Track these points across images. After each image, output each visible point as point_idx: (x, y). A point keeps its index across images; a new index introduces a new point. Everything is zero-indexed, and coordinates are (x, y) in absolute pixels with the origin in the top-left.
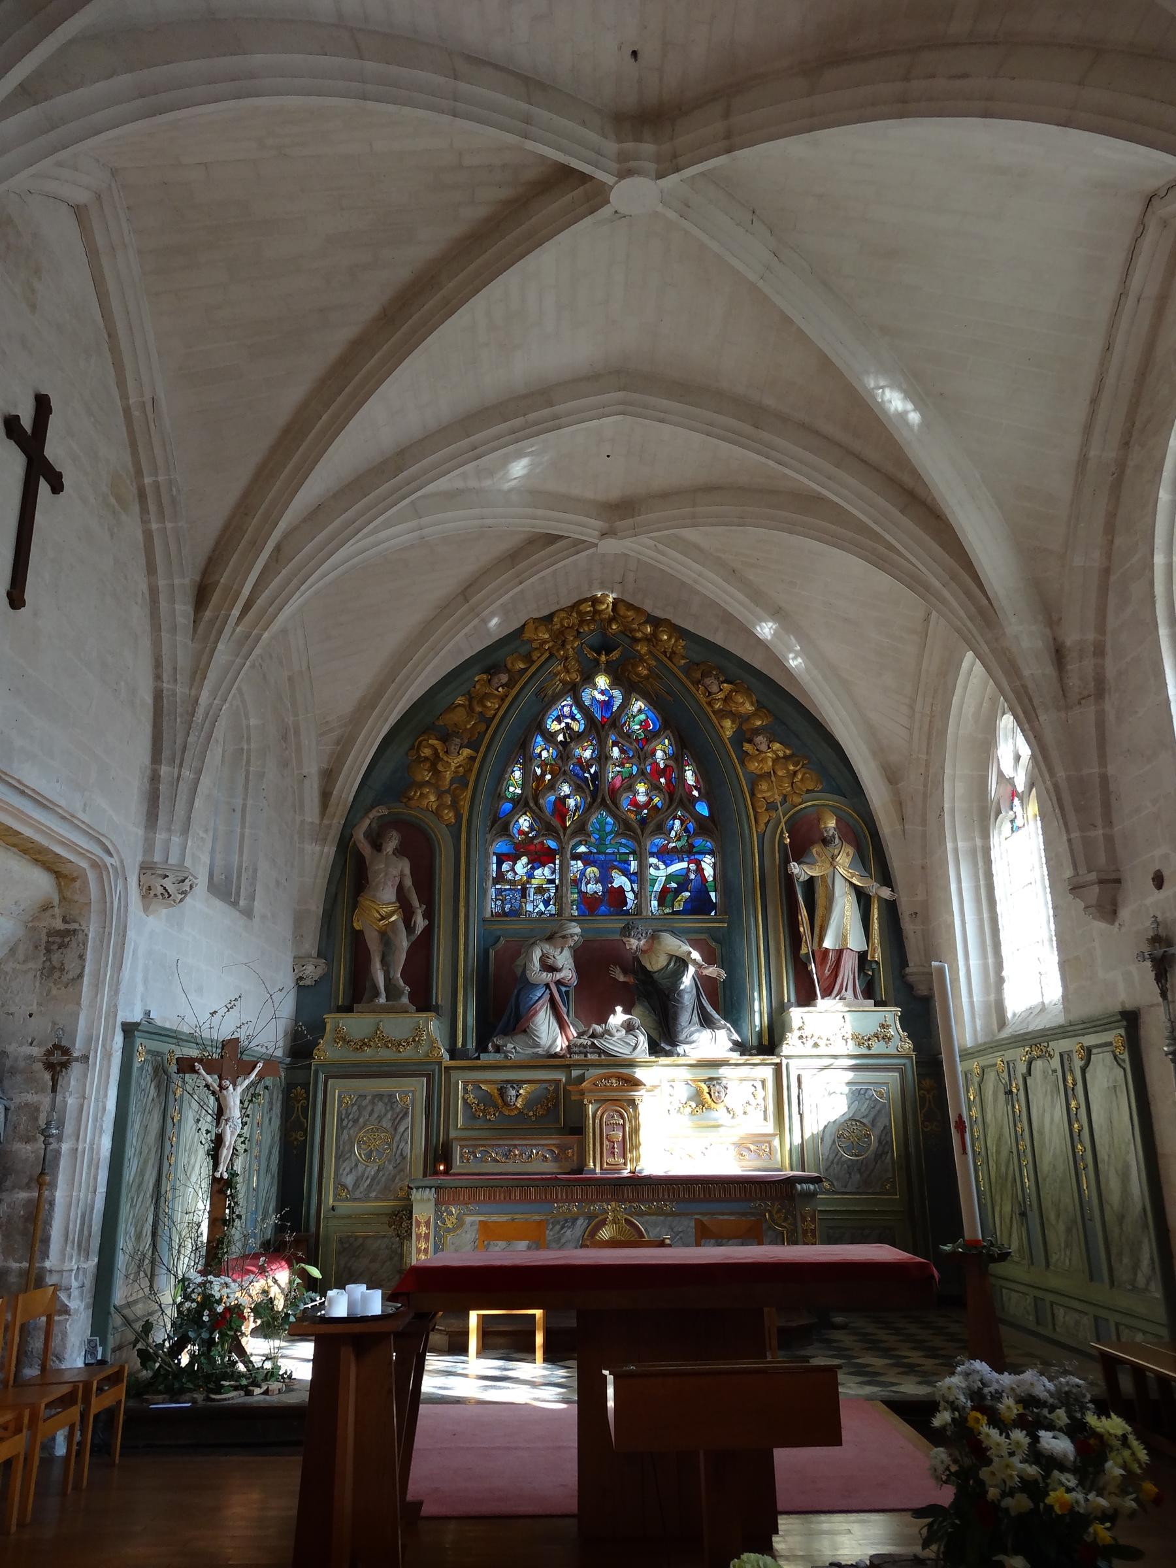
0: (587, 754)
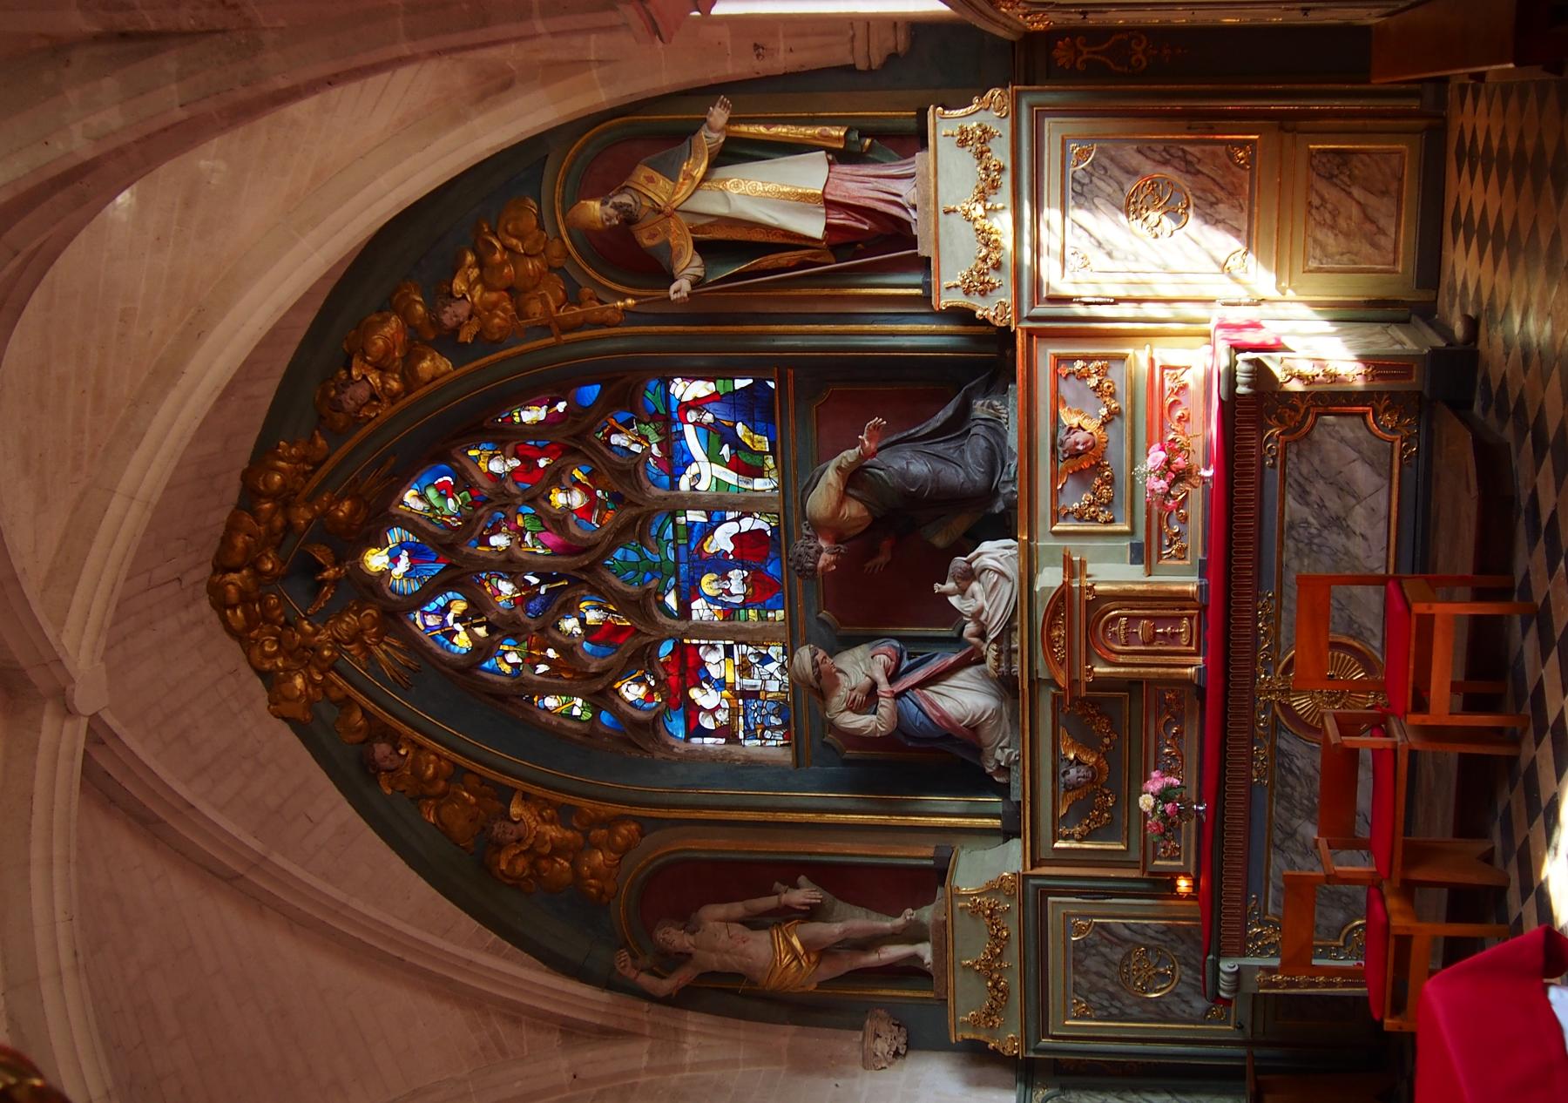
0: (506, 588)
